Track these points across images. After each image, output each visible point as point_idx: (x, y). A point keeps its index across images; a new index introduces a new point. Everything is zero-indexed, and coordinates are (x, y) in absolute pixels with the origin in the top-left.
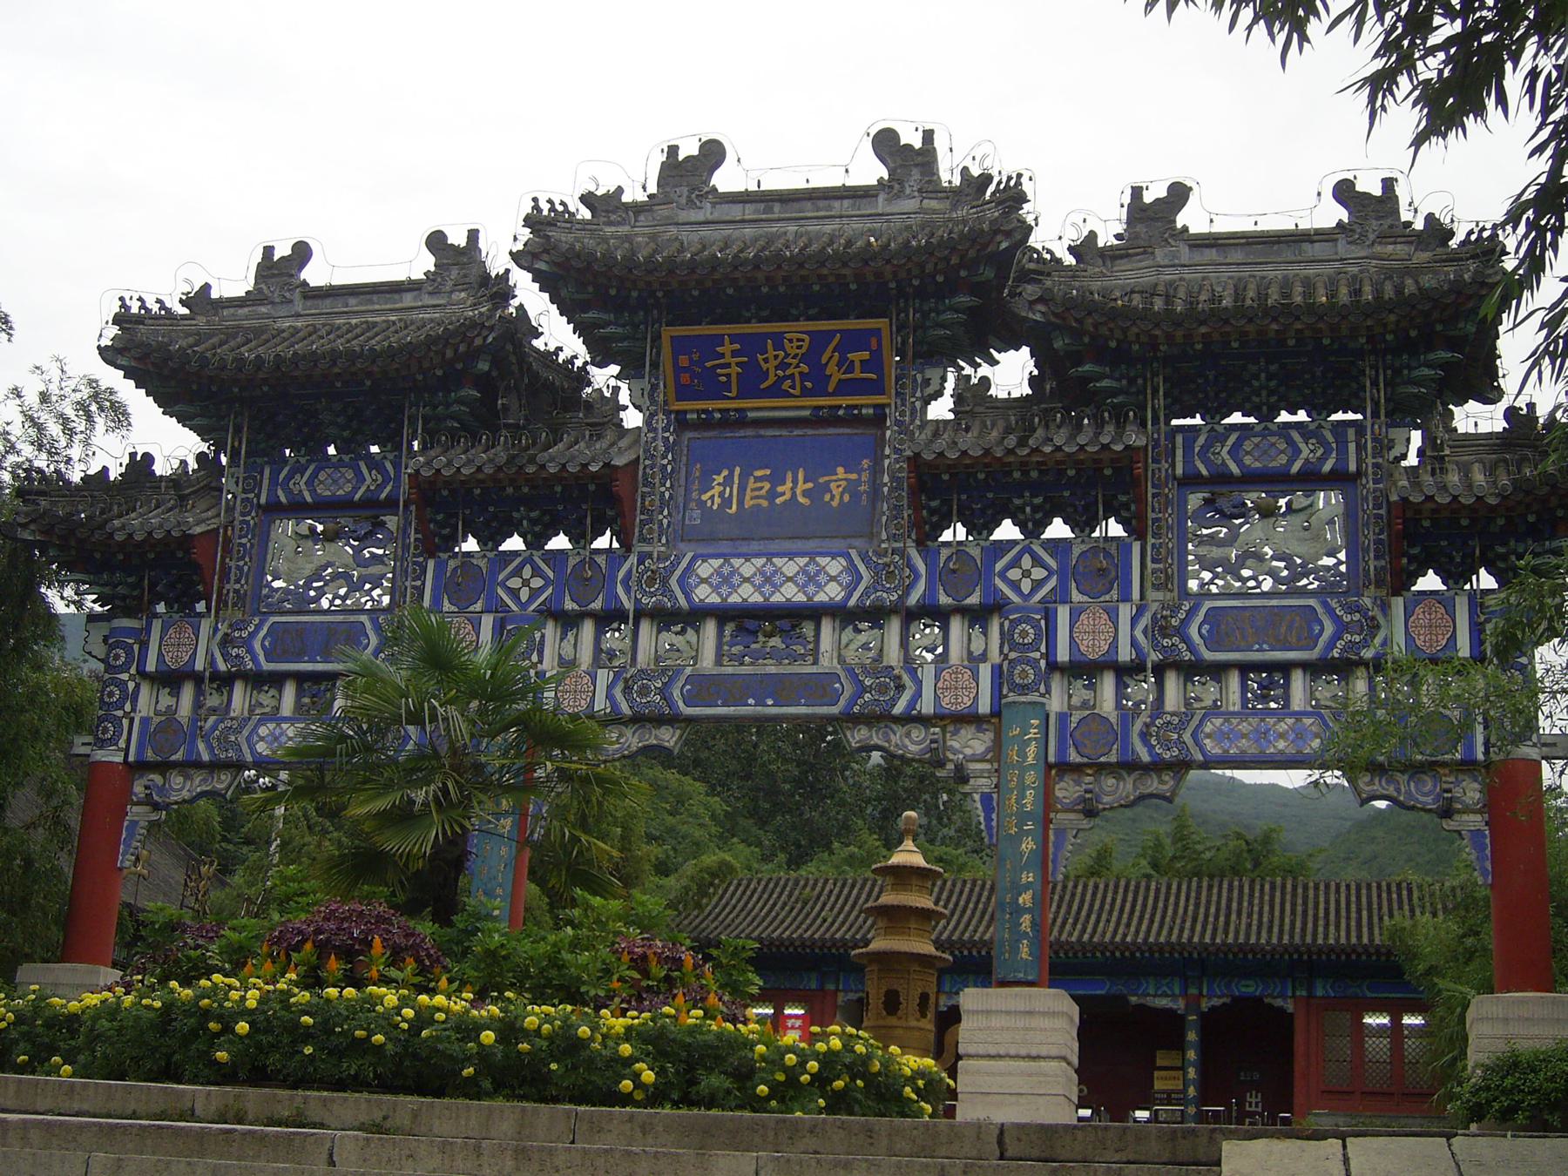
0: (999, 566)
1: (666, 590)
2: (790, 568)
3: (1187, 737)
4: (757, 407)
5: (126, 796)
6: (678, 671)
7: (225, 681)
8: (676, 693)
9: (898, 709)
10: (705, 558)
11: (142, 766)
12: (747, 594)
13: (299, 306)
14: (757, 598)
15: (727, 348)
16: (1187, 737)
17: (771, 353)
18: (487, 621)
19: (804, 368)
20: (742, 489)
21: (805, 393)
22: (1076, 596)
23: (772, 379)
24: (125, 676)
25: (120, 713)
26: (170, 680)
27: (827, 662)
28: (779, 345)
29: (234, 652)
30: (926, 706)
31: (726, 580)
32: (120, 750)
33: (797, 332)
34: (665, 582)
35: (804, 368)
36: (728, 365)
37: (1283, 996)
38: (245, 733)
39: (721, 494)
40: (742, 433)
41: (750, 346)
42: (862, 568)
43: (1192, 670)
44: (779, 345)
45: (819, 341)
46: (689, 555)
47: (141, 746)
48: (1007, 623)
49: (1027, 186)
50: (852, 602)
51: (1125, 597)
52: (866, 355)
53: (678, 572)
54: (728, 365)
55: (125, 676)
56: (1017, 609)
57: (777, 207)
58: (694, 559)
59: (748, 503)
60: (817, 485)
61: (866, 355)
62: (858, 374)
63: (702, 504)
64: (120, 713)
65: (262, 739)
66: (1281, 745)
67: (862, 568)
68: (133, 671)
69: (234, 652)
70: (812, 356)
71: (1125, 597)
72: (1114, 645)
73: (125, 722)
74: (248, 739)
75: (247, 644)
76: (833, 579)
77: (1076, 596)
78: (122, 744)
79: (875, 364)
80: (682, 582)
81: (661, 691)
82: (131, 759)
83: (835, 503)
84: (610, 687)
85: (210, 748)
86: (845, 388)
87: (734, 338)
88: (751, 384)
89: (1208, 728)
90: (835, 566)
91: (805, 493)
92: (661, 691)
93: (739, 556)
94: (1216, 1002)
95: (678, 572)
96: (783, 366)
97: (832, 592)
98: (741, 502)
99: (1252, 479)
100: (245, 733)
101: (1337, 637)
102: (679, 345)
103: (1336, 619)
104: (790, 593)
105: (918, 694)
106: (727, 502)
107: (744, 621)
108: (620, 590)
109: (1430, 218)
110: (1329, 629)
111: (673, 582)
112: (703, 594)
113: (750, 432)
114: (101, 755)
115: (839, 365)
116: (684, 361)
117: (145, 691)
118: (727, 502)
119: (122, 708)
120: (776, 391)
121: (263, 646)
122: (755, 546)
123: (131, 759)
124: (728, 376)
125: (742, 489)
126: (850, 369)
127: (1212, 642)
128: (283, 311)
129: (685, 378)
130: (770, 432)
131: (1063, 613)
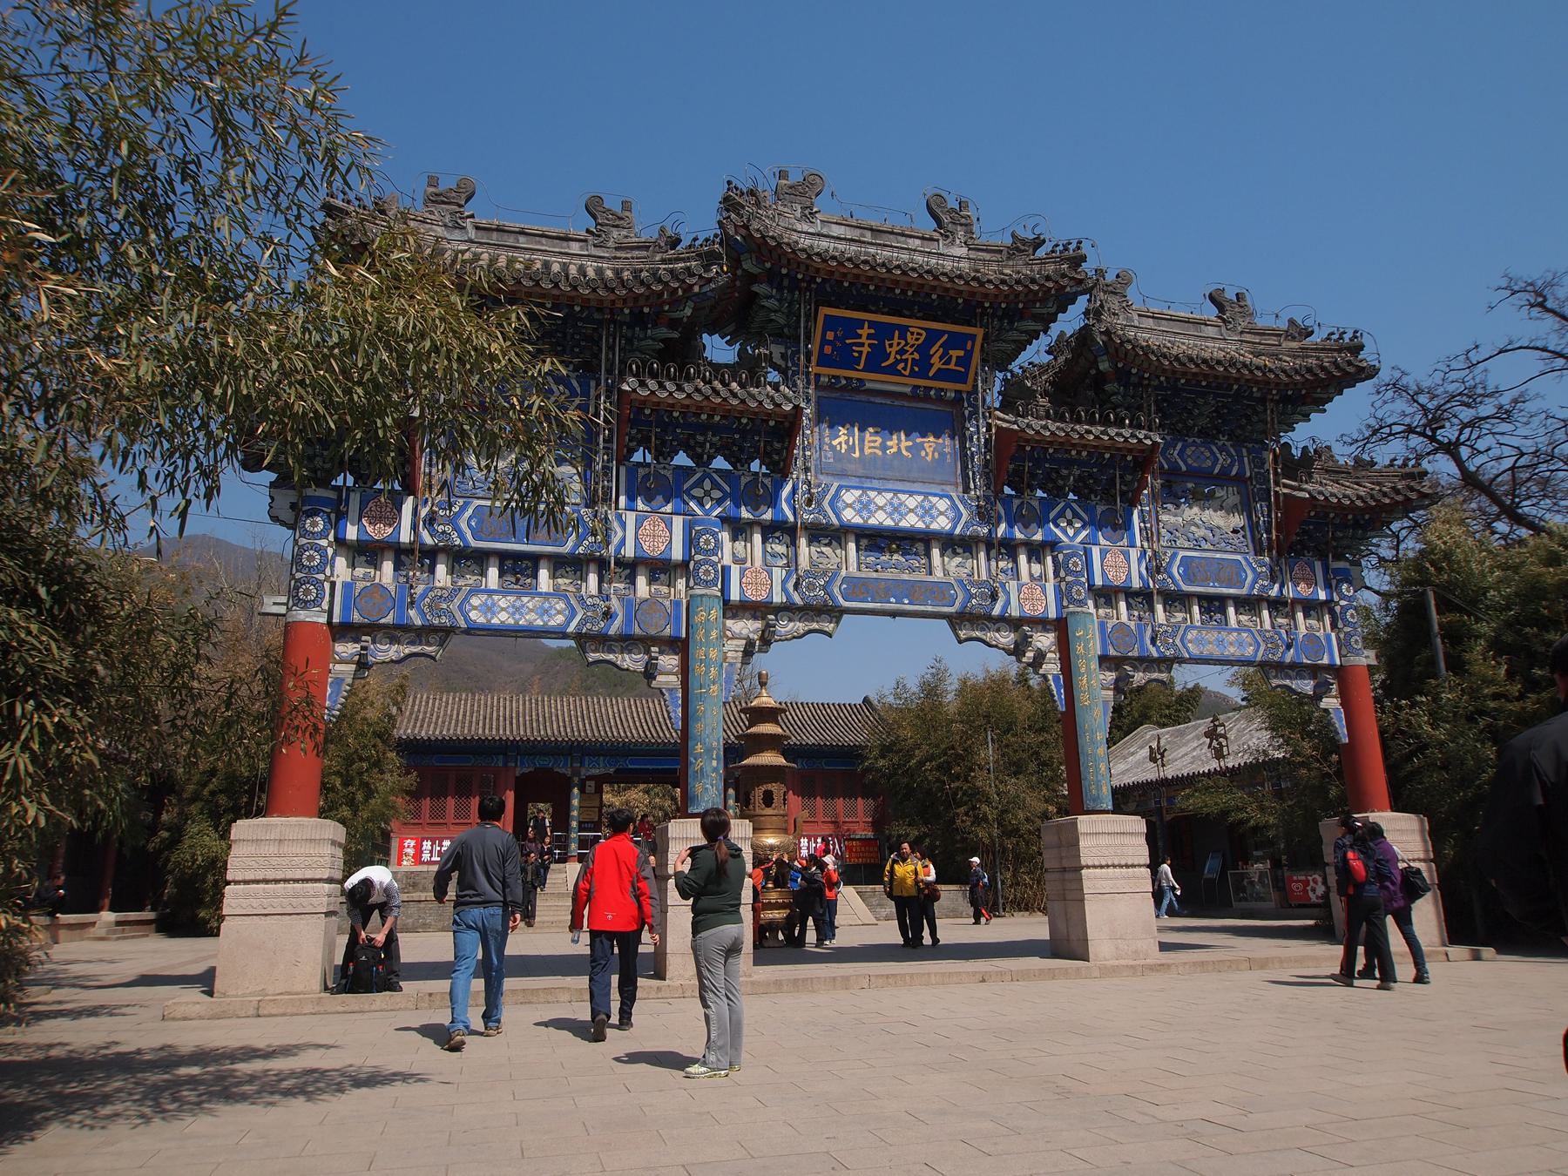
0: (1052, 515)
1: (821, 511)
2: (912, 502)
3: (1178, 641)
4: (874, 381)
5: (328, 657)
6: (835, 574)
7: (429, 556)
8: (836, 590)
9: (996, 611)
10: (848, 488)
11: (345, 631)
12: (881, 519)
13: (472, 234)
14: (889, 523)
15: (865, 332)
16: (1178, 641)
17: (896, 340)
18: (678, 522)
19: (916, 356)
20: (862, 441)
21: (913, 374)
22: (1102, 541)
23: (891, 360)
24: (324, 543)
25: (321, 577)
26: (367, 552)
27: (938, 574)
28: (903, 337)
29: (441, 528)
30: (1014, 612)
31: (865, 506)
32: (323, 611)
33: (917, 327)
34: (819, 504)
35: (916, 356)
36: (862, 345)
37: (565, 765)
38: (457, 601)
39: (847, 442)
40: (857, 398)
41: (882, 332)
42: (961, 507)
43: (1176, 600)
44: (903, 337)
45: (933, 336)
46: (836, 485)
47: (346, 608)
48: (1061, 557)
49: (1086, 249)
50: (957, 531)
51: (1133, 546)
52: (961, 353)
53: (829, 497)
54: (862, 345)
55: (324, 543)
56: (1069, 547)
57: (868, 234)
58: (840, 488)
59: (867, 451)
60: (915, 444)
61: (961, 353)
62: (952, 366)
63: (833, 448)
64: (321, 577)
65: (475, 608)
66: (1232, 650)
67: (961, 507)
68: (331, 537)
69: (441, 528)
70: (923, 350)
71: (1133, 546)
72: (1129, 576)
73: (327, 586)
74: (460, 607)
75: (453, 521)
76: (941, 513)
77: (1102, 541)
78: (325, 606)
79: (965, 361)
80: (832, 504)
81: (824, 588)
82: (336, 620)
83: (929, 458)
84: (784, 582)
85: (422, 614)
86: (942, 375)
87: (872, 324)
88: (875, 362)
89: (1189, 636)
90: (943, 505)
91: (908, 449)
92: (824, 588)
93: (904, 492)
94: (526, 770)
95: (829, 497)
96: (902, 352)
97: (942, 524)
98: (862, 450)
99: (1194, 474)
100: (457, 601)
101: (1255, 582)
102: (830, 322)
103: (1254, 570)
104: (911, 521)
105: (1008, 602)
106: (851, 449)
107: (876, 540)
108: (785, 506)
109: (1292, 322)
110: (1250, 577)
111: (826, 504)
112: (849, 516)
113: (863, 398)
114: (302, 615)
115: (941, 358)
116: (830, 336)
117: (341, 562)
118: (851, 449)
119: (323, 572)
120: (892, 370)
121: (469, 525)
122: (916, 487)
123: (336, 620)
124: (860, 353)
125: (862, 441)
126: (948, 362)
127: (1188, 577)
128: (457, 235)
129: (828, 350)
130: (878, 400)
131: (1096, 551)
